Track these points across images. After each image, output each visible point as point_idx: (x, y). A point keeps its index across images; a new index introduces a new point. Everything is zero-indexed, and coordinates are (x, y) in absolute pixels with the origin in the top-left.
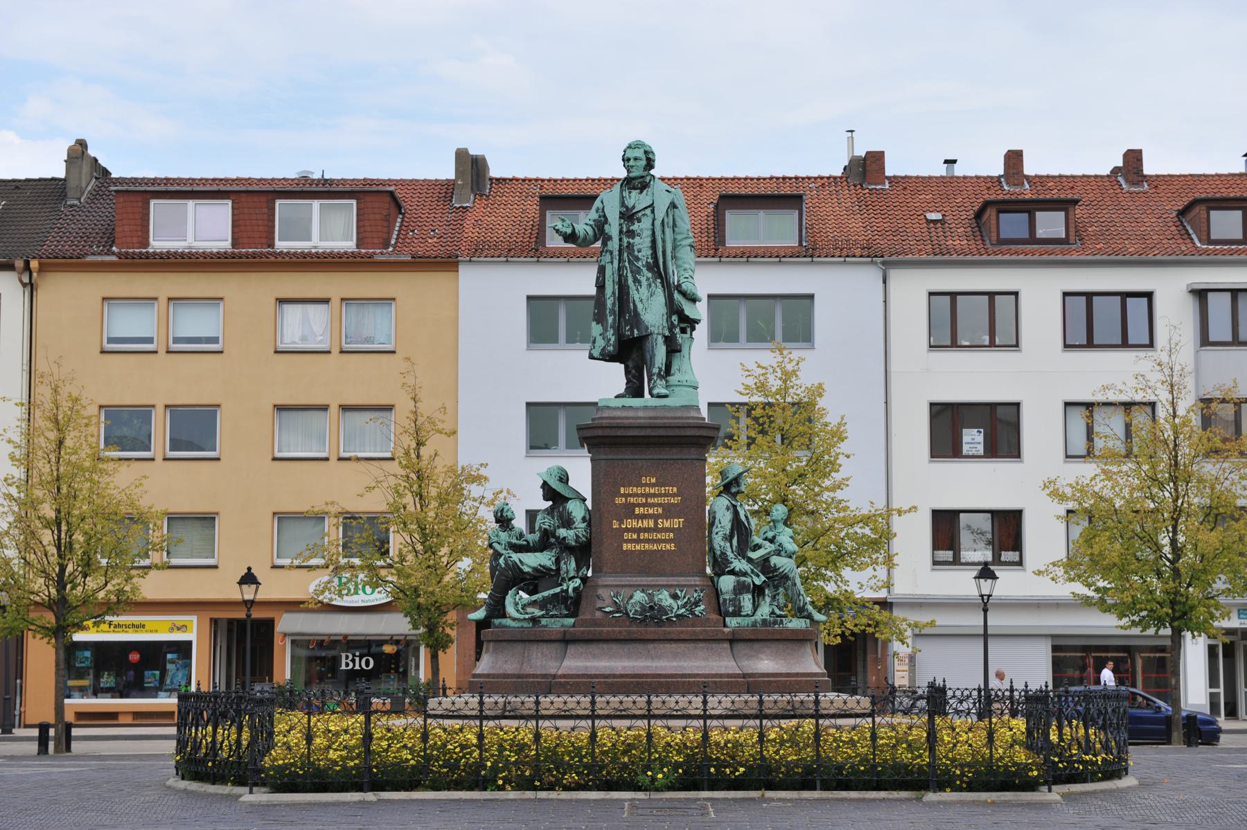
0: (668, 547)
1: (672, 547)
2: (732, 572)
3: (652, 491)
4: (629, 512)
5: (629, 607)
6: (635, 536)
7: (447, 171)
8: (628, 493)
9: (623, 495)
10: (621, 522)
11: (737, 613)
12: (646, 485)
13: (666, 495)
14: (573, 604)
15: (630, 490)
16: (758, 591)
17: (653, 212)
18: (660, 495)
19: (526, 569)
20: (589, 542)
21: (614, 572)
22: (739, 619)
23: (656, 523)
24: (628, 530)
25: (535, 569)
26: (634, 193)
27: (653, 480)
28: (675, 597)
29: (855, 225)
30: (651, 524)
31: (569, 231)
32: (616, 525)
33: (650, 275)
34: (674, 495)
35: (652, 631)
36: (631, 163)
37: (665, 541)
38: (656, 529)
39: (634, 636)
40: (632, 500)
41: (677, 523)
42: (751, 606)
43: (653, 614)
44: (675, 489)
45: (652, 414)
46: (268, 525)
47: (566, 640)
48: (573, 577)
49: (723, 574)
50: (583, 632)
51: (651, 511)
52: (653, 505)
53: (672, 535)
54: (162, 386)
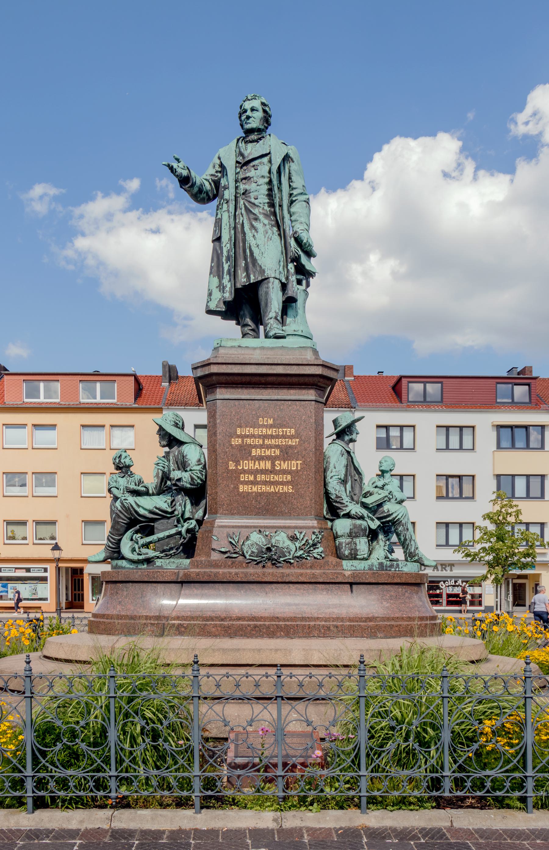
0: (285, 489)
1: (288, 489)
2: (348, 516)
3: (269, 433)
4: (244, 452)
5: (245, 549)
6: (252, 478)
7: (159, 372)
9: (238, 436)
10: (237, 463)
11: (353, 556)
12: (263, 426)
13: (284, 437)
14: (189, 548)
15: (248, 431)
16: (373, 535)
17: (270, 161)
18: (277, 437)
19: (142, 511)
20: (204, 482)
21: (231, 513)
22: (355, 563)
23: (273, 465)
24: (244, 472)
25: (151, 512)
26: (250, 145)
27: (271, 422)
28: (293, 538)
30: (268, 465)
31: (185, 173)
32: (232, 466)
33: (266, 222)
34: (291, 437)
36: (249, 113)
37: (282, 483)
38: (273, 471)
39: (251, 579)
40: (249, 441)
41: (295, 465)
42: (367, 550)
44: (293, 431)
46: (79, 526)
47: (184, 582)
48: (189, 519)
49: (338, 517)
50: (198, 574)
51: (268, 453)
52: (270, 447)
53: (289, 477)
54: (30, 463)
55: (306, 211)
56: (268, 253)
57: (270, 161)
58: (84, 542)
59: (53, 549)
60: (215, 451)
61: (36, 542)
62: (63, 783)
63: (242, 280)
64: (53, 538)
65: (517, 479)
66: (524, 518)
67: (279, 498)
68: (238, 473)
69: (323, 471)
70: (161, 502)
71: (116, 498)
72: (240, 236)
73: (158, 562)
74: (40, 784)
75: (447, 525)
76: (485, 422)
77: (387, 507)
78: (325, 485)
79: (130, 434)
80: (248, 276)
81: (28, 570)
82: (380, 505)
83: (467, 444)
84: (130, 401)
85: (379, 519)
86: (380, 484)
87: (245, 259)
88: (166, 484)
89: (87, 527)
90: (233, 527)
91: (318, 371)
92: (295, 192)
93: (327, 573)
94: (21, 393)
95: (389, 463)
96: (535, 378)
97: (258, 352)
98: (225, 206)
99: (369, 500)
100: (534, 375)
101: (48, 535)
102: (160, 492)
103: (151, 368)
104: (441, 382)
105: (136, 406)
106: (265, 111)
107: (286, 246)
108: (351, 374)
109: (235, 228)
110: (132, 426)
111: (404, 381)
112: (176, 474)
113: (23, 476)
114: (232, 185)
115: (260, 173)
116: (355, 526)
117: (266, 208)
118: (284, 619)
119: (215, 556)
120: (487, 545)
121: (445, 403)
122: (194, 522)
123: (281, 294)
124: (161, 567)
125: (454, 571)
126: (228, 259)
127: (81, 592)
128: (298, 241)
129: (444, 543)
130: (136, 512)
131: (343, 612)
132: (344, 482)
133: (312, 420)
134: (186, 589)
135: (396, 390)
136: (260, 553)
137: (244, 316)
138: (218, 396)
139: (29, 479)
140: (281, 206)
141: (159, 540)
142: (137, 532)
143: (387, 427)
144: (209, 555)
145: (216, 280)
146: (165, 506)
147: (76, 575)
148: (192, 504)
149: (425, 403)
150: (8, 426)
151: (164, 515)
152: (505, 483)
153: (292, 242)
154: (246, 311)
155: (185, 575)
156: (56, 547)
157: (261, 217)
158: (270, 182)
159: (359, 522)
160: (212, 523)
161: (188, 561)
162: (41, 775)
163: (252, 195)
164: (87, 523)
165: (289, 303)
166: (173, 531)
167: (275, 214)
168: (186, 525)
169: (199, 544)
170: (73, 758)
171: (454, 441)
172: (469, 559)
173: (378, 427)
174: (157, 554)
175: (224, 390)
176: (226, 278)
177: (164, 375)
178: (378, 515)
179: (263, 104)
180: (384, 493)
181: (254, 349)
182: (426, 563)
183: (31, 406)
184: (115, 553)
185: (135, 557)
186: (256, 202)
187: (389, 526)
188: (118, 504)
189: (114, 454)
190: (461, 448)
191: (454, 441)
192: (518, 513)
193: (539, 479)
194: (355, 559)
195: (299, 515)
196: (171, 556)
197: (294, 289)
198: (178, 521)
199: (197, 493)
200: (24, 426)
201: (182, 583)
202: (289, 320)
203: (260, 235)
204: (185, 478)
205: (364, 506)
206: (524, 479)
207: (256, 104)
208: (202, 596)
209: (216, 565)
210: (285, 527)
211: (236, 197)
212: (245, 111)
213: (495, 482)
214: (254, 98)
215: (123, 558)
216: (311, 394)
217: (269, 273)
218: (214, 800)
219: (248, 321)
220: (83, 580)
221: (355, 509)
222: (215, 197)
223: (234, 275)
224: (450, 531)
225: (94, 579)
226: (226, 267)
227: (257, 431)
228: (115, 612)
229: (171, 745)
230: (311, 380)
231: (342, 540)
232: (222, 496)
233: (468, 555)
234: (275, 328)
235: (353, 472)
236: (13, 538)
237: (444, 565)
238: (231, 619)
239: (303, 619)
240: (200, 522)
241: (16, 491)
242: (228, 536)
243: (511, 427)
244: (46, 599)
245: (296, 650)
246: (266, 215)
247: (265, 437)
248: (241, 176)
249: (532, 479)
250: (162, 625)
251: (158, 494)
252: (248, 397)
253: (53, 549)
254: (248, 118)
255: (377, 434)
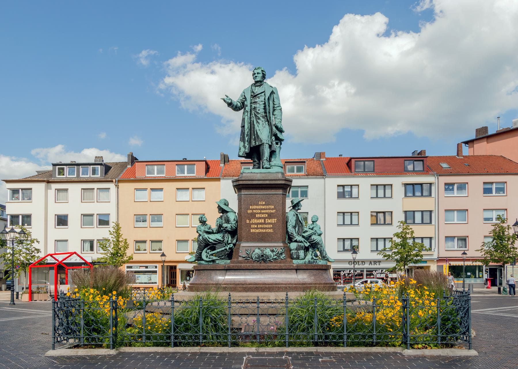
0: (270, 231)
1: (271, 231)
2: (296, 241)
5: (253, 255)
6: (256, 226)
7: (219, 158)
8: (254, 208)
9: (251, 209)
10: (250, 220)
11: (298, 258)
12: (261, 205)
13: (269, 209)
14: (230, 255)
16: (306, 249)
17: (265, 95)
18: (267, 209)
19: (211, 241)
20: (237, 228)
21: (247, 241)
22: (298, 261)
23: (265, 221)
24: (253, 224)
25: (214, 241)
26: (257, 88)
27: (264, 203)
28: (273, 251)
29: (318, 169)
30: (263, 221)
31: (230, 101)
33: (263, 120)
34: (272, 209)
35: (263, 265)
36: (256, 75)
37: (269, 228)
38: (265, 223)
39: (255, 268)
40: (255, 211)
43: (263, 258)
44: (273, 207)
45: (264, 175)
46: (175, 243)
47: (227, 270)
49: (292, 242)
50: (233, 266)
51: (263, 216)
52: (263, 213)
53: (271, 226)
54: (149, 210)
55: (280, 114)
56: (263, 132)
57: (265, 95)
58: (177, 252)
59: (162, 256)
60: (241, 215)
61: (151, 252)
62: (184, 338)
63: (253, 144)
64: (160, 250)
65: (416, 213)
66: (415, 235)
67: (267, 234)
68: (250, 224)
69: (286, 223)
70: (219, 236)
71: (200, 235)
72: (252, 126)
73: (217, 262)
74: (176, 338)
75: (377, 239)
76: (397, 182)
77: (313, 237)
78: (287, 228)
79: (203, 192)
80: (255, 143)
81: (147, 267)
82: (310, 236)
83: (388, 194)
84: (203, 175)
85: (309, 242)
86: (311, 227)
87: (254, 135)
88: (220, 229)
89: (179, 243)
90: (248, 247)
91: (283, 182)
92: (276, 106)
93: (287, 265)
94: (145, 172)
95: (316, 218)
96: (426, 157)
97: (259, 174)
98: (246, 113)
99: (305, 235)
100: (426, 155)
101: (158, 248)
102: (218, 232)
103: (214, 157)
104: (373, 161)
105: (206, 177)
106: (263, 74)
107: (271, 129)
108: (324, 157)
109: (250, 123)
110: (204, 188)
111: (353, 161)
112: (225, 225)
113: (145, 216)
114: (249, 105)
115: (260, 100)
116: (298, 245)
117: (263, 114)
118: (268, 284)
119: (240, 259)
120: (396, 250)
121: (376, 172)
122: (232, 245)
123: (269, 149)
124: (218, 264)
125: (381, 265)
126: (247, 135)
127: (174, 279)
128: (277, 127)
129: (375, 250)
130: (208, 241)
131: (290, 281)
132: (295, 227)
133: (281, 202)
134: (228, 273)
135: (349, 165)
136: (259, 257)
137: (254, 158)
138: (242, 193)
139: (148, 218)
140: (269, 113)
141: (218, 252)
142: (208, 249)
143: (343, 186)
144: (238, 258)
145: (242, 143)
146: (220, 238)
147: (172, 270)
148: (231, 237)
149: (365, 173)
150: (137, 189)
151: (219, 242)
152: (409, 215)
153: (274, 128)
154: (255, 156)
155: (228, 266)
156: (163, 255)
157: (261, 118)
158: (265, 104)
159: (300, 244)
160: (240, 245)
161: (229, 261)
162: (176, 334)
163: (257, 109)
164: (179, 241)
165: (272, 153)
166: (223, 249)
167: (266, 116)
168: (229, 246)
169: (234, 253)
170: (187, 330)
171: (381, 193)
172: (386, 258)
173: (338, 186)
174: (217, 258)
175: (245, 191)
176: (246, 143)
177: (221, 160)
178: (309, 241)
179: (262, 71)
180: (311, 231)
181: (257, 173)
182: (330, 260)
183: (150, 178)
184: (199, 258)
185: (208, 260)
186: (259, 112)
187: (314, 245)
188: (201, 238)
189: (199, 216)
190: (385, 197)
191: (381, 193)
192: (412, 232)
193: (429, 213)
194: (299, 259)
195: (275, 242)
196: (223, 259)
197: (275, 147)
198: (226, 245)
199: (233, 233)
200: (146, 189)
201: (227, 270)
202: (272, 159)
203: (260, 125)
204: (228, 226)
205: (303, 237)
206: (420, 213)
207: (259, 71)
208: (233, 275)
209: (241, 262)
210: (269, 246)
211: (251, 110)
212: (255, 74)
213: (404, 215)
214: (259, 68)
215: (203, 260)
216: (280, 192)
217: (264, 141)
218: (235, 344)
219: (256, 160)
220: (176, 272)
221: (299, 238)
222: (242, 108)
223: (250, 142)
224: (379, 242)
225: (182, 271)
226: (246, 139)
227: (258, 207)
228: (199, 282)
229: (221, 325)
230: (280, 186)
231: (293, 251)
232: (244, 234)
233: (385, 256)
234: (267, 165)
235: (299, 223)
236: (139, 250)
237: (375, 262)
238: (246, 284)
239: (276, 284)
240: (234, 245)
241: (141, 224)
242: (246, 250)
243: (413, 185)
244: (156, 283)
245: (272, 296)
246: (263, 117)
247: (261, 209)
248: (253, 101)
249: (424, 213)
250: (218, 287)
251: (217, 233)
252: (255, 193)
253: (162, 256)
254: (256, 77)
255: (338, 189)
